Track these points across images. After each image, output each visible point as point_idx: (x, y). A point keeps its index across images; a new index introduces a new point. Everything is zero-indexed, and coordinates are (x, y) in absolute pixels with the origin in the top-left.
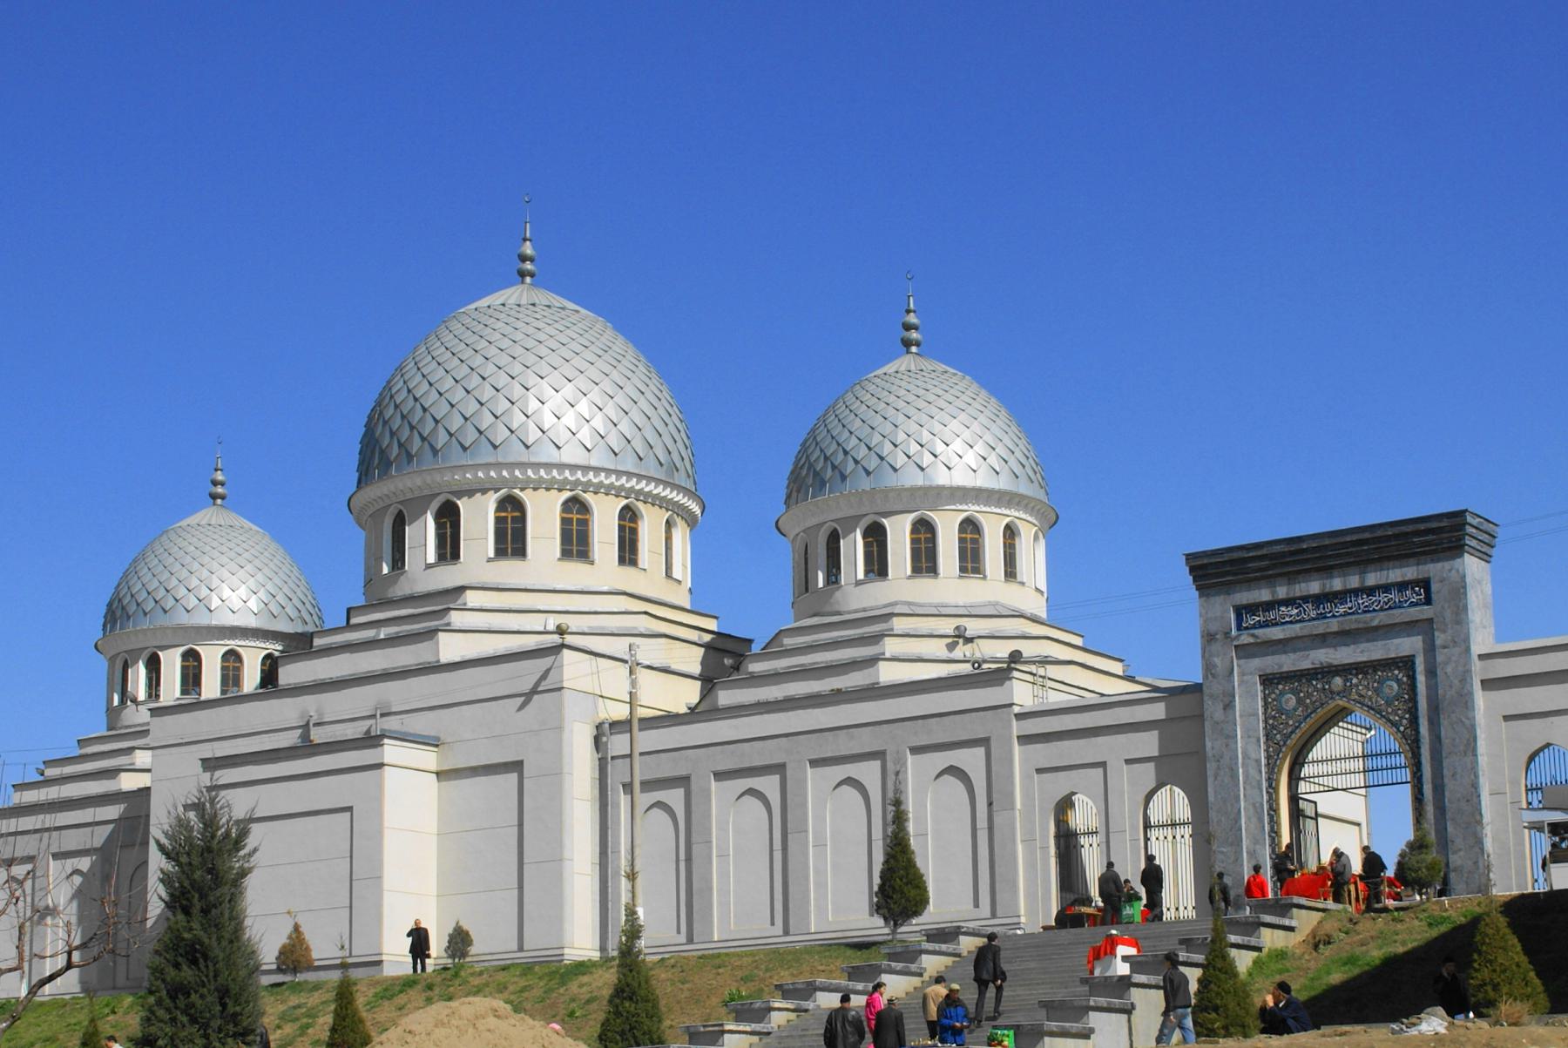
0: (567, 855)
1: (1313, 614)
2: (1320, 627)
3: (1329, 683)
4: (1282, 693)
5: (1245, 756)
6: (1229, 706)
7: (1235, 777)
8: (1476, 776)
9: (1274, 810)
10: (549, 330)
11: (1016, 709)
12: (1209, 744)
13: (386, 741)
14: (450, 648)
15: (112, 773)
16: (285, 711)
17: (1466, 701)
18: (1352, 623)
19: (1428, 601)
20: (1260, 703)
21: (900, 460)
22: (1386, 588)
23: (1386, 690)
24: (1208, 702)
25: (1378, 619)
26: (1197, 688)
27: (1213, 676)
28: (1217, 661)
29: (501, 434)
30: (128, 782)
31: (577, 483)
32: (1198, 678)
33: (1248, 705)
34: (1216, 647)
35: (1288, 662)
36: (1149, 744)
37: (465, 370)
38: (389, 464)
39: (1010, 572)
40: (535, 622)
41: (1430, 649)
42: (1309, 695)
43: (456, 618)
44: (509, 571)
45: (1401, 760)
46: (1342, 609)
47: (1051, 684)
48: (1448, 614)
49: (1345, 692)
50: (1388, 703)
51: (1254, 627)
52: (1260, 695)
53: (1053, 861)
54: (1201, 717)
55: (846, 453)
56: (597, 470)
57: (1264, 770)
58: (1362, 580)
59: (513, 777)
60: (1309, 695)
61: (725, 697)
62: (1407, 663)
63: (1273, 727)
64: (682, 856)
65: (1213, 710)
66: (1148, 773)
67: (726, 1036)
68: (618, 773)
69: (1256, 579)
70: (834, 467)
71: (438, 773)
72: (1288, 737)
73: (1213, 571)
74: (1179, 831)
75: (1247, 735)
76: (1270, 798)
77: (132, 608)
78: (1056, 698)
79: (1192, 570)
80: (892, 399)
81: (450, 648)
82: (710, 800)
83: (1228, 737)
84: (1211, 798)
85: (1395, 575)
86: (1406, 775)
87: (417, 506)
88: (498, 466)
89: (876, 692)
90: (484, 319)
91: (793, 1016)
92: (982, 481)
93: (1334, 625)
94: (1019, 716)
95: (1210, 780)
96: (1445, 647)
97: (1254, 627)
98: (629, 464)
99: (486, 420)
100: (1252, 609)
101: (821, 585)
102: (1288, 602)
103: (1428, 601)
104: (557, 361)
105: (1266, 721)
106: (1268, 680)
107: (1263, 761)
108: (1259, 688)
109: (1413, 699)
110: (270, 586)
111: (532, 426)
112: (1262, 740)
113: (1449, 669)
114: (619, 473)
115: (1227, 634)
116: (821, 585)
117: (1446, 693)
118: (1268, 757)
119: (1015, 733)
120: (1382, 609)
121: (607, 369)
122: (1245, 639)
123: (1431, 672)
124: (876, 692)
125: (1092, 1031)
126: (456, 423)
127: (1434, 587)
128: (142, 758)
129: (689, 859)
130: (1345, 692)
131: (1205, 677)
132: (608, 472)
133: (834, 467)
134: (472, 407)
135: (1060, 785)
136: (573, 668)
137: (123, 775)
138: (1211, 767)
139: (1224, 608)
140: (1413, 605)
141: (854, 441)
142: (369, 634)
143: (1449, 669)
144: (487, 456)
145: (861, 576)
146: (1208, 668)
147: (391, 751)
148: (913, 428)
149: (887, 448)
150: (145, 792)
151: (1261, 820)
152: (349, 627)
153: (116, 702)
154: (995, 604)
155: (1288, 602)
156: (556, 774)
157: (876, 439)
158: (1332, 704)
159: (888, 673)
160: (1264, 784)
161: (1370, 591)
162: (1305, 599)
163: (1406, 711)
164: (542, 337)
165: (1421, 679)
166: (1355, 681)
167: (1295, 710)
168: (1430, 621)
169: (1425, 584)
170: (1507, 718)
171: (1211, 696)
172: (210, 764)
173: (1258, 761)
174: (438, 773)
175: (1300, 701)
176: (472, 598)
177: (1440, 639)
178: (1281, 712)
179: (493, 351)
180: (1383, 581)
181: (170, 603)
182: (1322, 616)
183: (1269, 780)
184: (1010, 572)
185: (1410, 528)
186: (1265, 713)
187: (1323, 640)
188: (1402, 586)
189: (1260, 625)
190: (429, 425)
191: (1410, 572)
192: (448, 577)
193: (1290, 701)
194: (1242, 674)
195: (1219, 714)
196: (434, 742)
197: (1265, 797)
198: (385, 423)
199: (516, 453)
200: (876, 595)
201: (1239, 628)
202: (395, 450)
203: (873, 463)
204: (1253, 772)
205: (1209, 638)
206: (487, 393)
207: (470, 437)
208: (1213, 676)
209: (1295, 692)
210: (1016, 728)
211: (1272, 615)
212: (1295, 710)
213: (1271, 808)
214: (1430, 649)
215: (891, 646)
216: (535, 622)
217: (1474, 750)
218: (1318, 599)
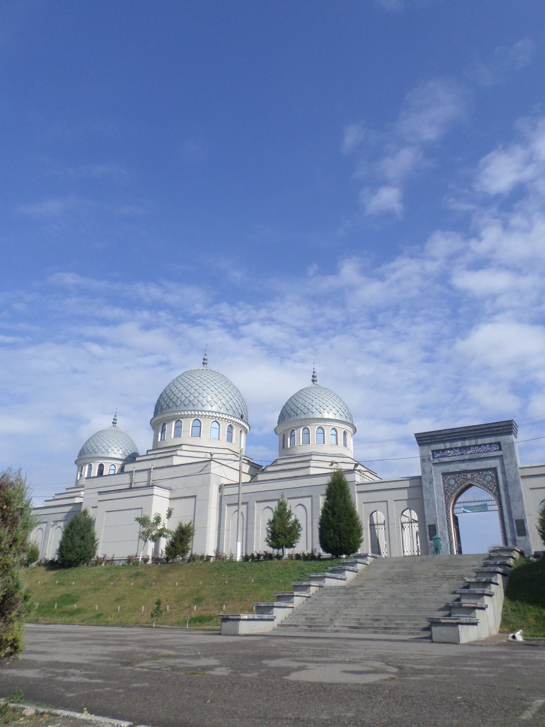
0: (208, 525)
1: (459, 453)
2: (462, 458)
3: (466, 476)
4: (449, 479)
5: (438, 500)
6: (431, 483)
7: (434, 506)
8: (524, 508)
9: (448, 518)
10: (211, 376)
11: (357, 483)
12: (424, 496)
13: (155, 487)
14: (176, 461)
15: (74, 497)
16: (125, 479)
17: (517, 482)
18: (475, 456)
19: (500, 449)
20: (442, 482)
21: (314, 410)
22: (485, 445)
23: (487, 479)
24: (424, 482)
25: (483, 455)
26: (420, 478)
27: (425, 473)
28: (426, 468)
29: (196, 402)
30: (77, 500)
31: (216, 417)
32: (420, 474)
33: (438, 483)
34: (426, 463)
35: (451, 468)
36: (404, 494)
37: (187, 384)
38: (163, 409)
39: (345, 445)
40: (203, 455)
41: (503, 465)
42: (459, 480)
43: (179, 453)
44: (196, 441)
45: (494, 502)
46: (469, 452)
47: (365, 476)
48: (508, 454)
49: (472, 479)
50: (488, 483)
51: (439, 457)
52: (442, 480)
53: (369, 533)
54: (421, 486)
55: (298, 408)
56: (222, 414)
57: (444, 505)
58: (476, 442)
59: (193, 499)
60: (459, 480)
61: (260, 477)
62: (494, 470)
63: (447, 490)
64: (245, 527)
65: (425, 484)
66: (405, 505)
67: (295, 598)
68: (225, 501)
69: (439, 442)
70: (294, 412)
71: (170, 499)
72: (452, 493)
73: (423, 439)
74: (413, 524)
75: (438, 493)
76: (447, 514)
77: (86, 451)
78: (366, 481)
79: (417, 438)
80: (311, 394)
81: (176, 461)
82: (254, 510)
83: (431, 493)
84: (426, 514)
85: (488, 440)
86: (497, 508)
87: (170, 420)
88: (194, 411)
89: (309, 476)
90: (193, 372)
91: (318, 588)
92: (338, 417)
93: (467, 457)
94: (357, 485)
95: (425, 507)
96: (508, 464)
97: (439, 457)
98: (231, 413)
99: (192, 398)
100: (438, 451)
101: (289, 446)
102: (450, 449)
103: (500, 449)
104: (213, 389)
105: (444, 488)
106: (444, 474)
107: (444, 502)
108: (441, 477)
109: (498, 483)
110: (126, 448)
111: (205, 400)
112: (443, 494)
113: (510, 472)
114: (229, 415)
115: (429, 460)
116: (289, 446)
117: (510, 480)
118: (446, 500)
119: (356, 491)
120: (484, 452)
121: (227, 387)
122: (436, 461)
123: (504, 473)
124: (309, 476)
125: (487, 606)
126: (183, 398)
127: (502, 444)
128: (82, 493)
129: (247, 529)
130: (472, 479)
131: (422, 474)
132: (226, 414)
133: (294, 412)
134: (188, 394)
135: (372, 507)
136: (214, 467)
137: (76, 498)
138: (426, 503)
139: (428, 450)
140: (495, 451)
141: (300, 405)
142: (153, 457)
143: (510, 472)
144: (191, 407)
145: (301, 444)
146: (423, 471)
147: (156, 491)
148: (317, 401)
149: (310, 407)
150: (81, 503)
151: (444, 522)
152: (147, 455)
153: (78, 478)
154: (341, 454)
155: (450, 449)
156: (206, 500)
157: (307, 404)
158: (467, 483)
159: (313, 471)
160: (445, 510)
161: (480, 446)
162: (456, 448)
163: (494, 486)
164: (209, 377)
165: (500, 475)
166: (475, 476)
167: (454, 485)
168: (502, 456)
169: (499, 444)
170: (531, 489)
171: (425, 479)
172: (100, 493)
173: (442, 502)
174: (170, 499)
175: (456, 482)
176: (184, 447)
177: (506, 462)
178: (449, 485)
179: (194, 384)
180: (484, 443)
181: (97, 450)
182: (462, 454)
183: (447, 508)
184: (345, 445)
185: (493, 425)
186: (444, 485)
187: (463, 461)
188: (491, 444)
189: (441, 457)
190: (175, 399)
191: (493, 440)
192: (177, 442)
193: (452, 482)
194: (435, 473)
195: (428, 485)
196: (170, 489)
197: (445, 514)
198: (165, 401)
199: (200, 407)
200: (306, 449)
201: (433, 457)
202: (165, 406)
203: (306, 411)
204: (441, 505)
205: (423, 460)
206: (193, 391)
207: (187, 402)
208: (425, 473)
209: (454, 479)
210: (356, 489)
211: (445, 453)
212: (454, 485)
213: (447, 518)
214: (503, 465)
215: (312, 464)
216: (203, 455)
217: (522, 499)
218: (461, 448)
